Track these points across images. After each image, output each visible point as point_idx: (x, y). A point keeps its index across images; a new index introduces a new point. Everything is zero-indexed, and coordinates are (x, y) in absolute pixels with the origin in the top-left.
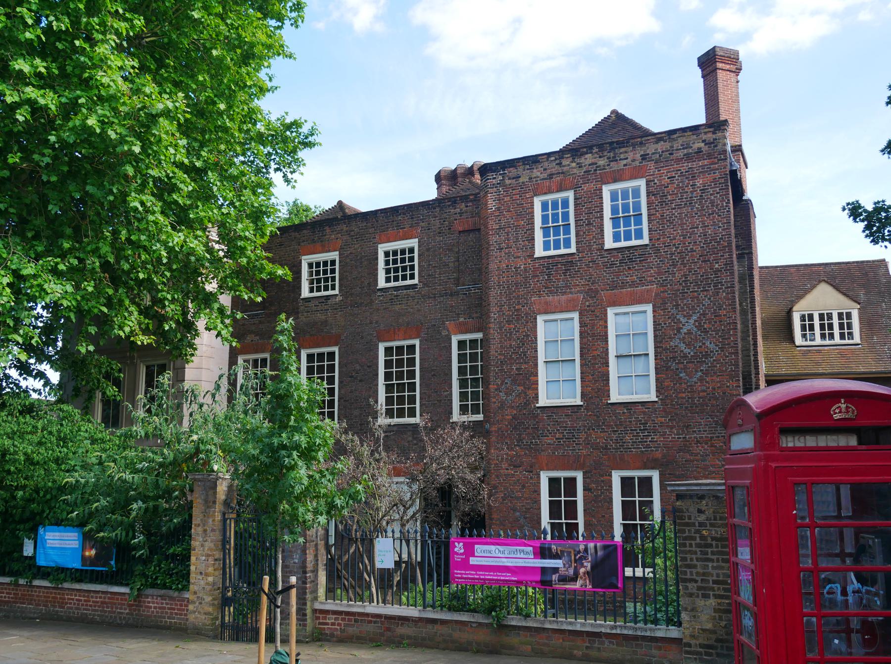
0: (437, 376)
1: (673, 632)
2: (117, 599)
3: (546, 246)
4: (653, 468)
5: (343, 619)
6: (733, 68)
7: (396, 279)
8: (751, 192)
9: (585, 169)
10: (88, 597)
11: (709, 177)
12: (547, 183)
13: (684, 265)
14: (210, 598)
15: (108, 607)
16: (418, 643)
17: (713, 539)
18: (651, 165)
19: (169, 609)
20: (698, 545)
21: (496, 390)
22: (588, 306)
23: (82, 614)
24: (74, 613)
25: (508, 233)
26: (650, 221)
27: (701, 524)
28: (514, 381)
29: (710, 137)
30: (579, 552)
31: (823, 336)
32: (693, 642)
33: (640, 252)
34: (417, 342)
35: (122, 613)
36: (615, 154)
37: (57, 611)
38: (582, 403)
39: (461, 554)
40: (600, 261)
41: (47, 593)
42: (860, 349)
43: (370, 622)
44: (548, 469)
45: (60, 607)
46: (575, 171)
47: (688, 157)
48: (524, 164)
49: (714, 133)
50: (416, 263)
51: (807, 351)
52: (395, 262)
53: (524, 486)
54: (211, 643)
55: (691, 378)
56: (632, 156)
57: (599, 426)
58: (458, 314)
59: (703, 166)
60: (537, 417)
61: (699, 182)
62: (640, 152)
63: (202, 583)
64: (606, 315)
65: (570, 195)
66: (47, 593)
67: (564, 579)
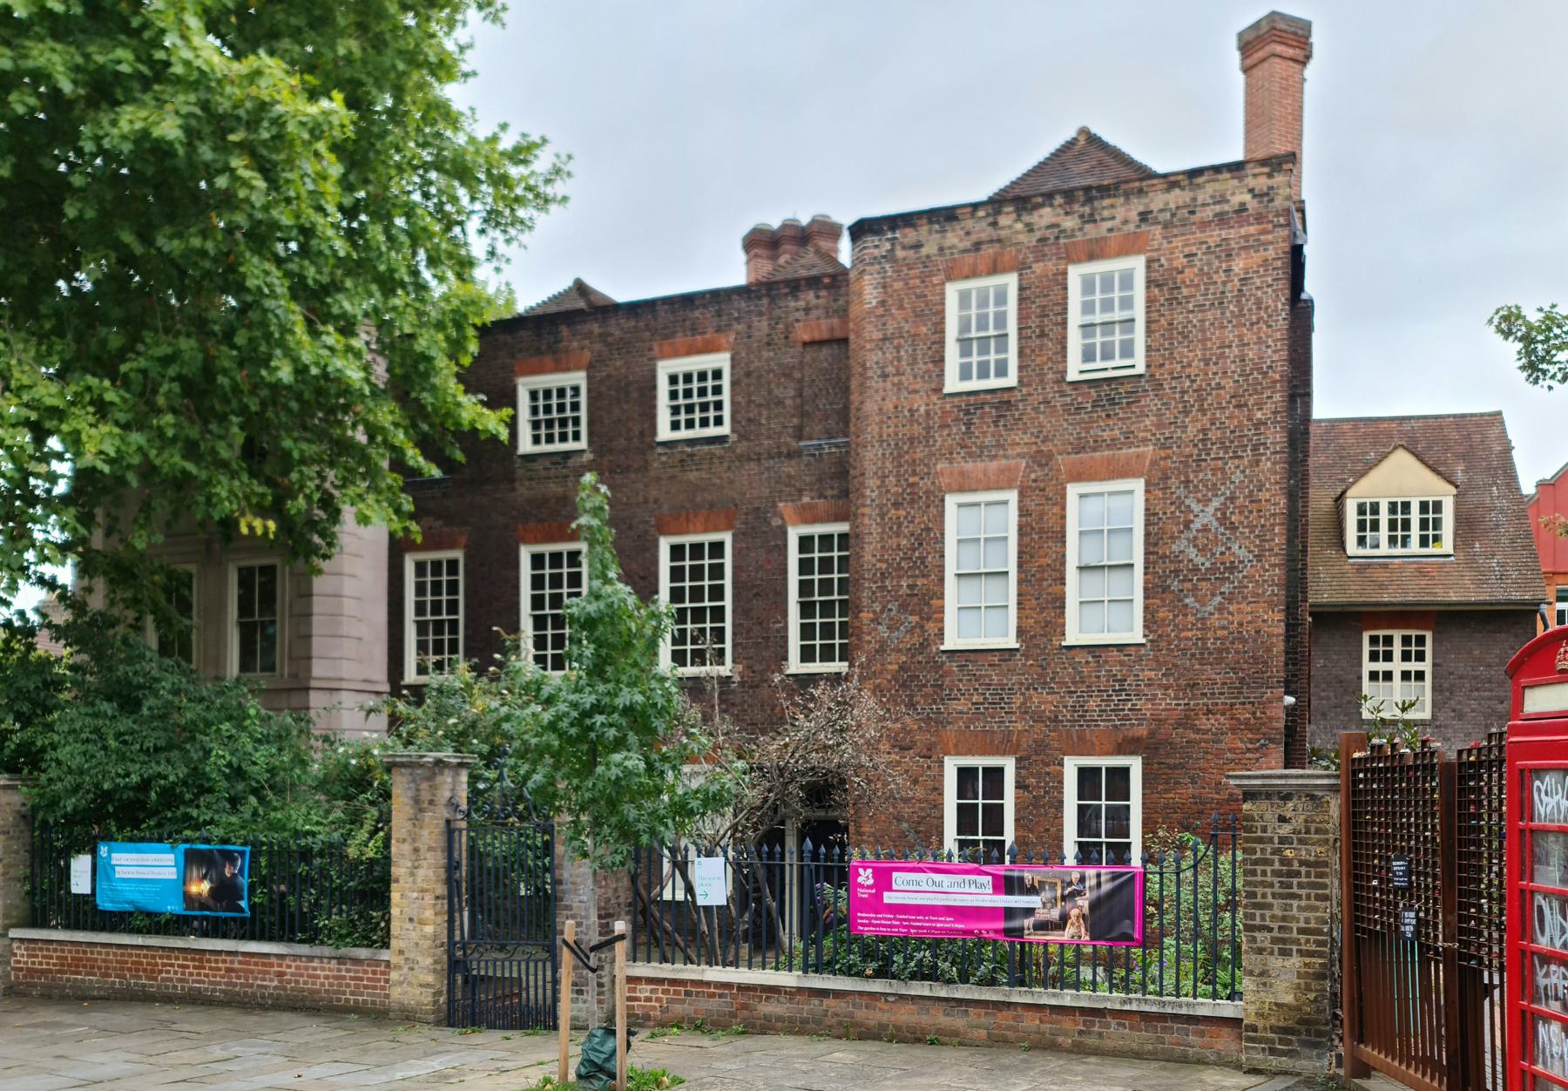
0: (761, 595)
1: (1227, 1009)
2: (131, 955)
3: (965, 374)
4: (1132, 753)
5: (665, 992)
6: (1297, 53)
7: (690, 424)
8: (1311, 288)
9: (1038, 235)
10: (201, 960)
11: (1256, 257)
12: (969, 258)
13: (1202, 411)
14: (429, 961)
15: (238, 978)
16: (798, 1027)
17: (1302, 863)
18: (1157, 231)
19: (352, 978)
20: (1276, 873)
22: (1035, 481)
23: (190, 989)
24: (175, 987)
26: (1149, 332)
27: (1282, 840)
28: (903, 607)
29: (1262, 183)
31: (1392, 541)
32: (1260, 1024)
33: (1128, 387)
34: (727, 538)
35: (266, 987)
36: (1093, 209)
37: (144, 986)
39: (869, 887)
40: (1058, 402)
41: (122, 955)
43: (712, 995)
44: (958, 754)
45: (148, 978)
46: (1023, 238)
48: (931, 222)
49: (1270, 176)
50: (726, 396)
51: (1364, 567)
54: (1115, 1066)
55: (1204, 605)
56: (1121, 213)
59: (1246, 237)
62: (1137, 205)
63: (414, 935)
64: (1064, 497)
65: (1011, 281)
66: (122, 955)
67: (1042, 926)
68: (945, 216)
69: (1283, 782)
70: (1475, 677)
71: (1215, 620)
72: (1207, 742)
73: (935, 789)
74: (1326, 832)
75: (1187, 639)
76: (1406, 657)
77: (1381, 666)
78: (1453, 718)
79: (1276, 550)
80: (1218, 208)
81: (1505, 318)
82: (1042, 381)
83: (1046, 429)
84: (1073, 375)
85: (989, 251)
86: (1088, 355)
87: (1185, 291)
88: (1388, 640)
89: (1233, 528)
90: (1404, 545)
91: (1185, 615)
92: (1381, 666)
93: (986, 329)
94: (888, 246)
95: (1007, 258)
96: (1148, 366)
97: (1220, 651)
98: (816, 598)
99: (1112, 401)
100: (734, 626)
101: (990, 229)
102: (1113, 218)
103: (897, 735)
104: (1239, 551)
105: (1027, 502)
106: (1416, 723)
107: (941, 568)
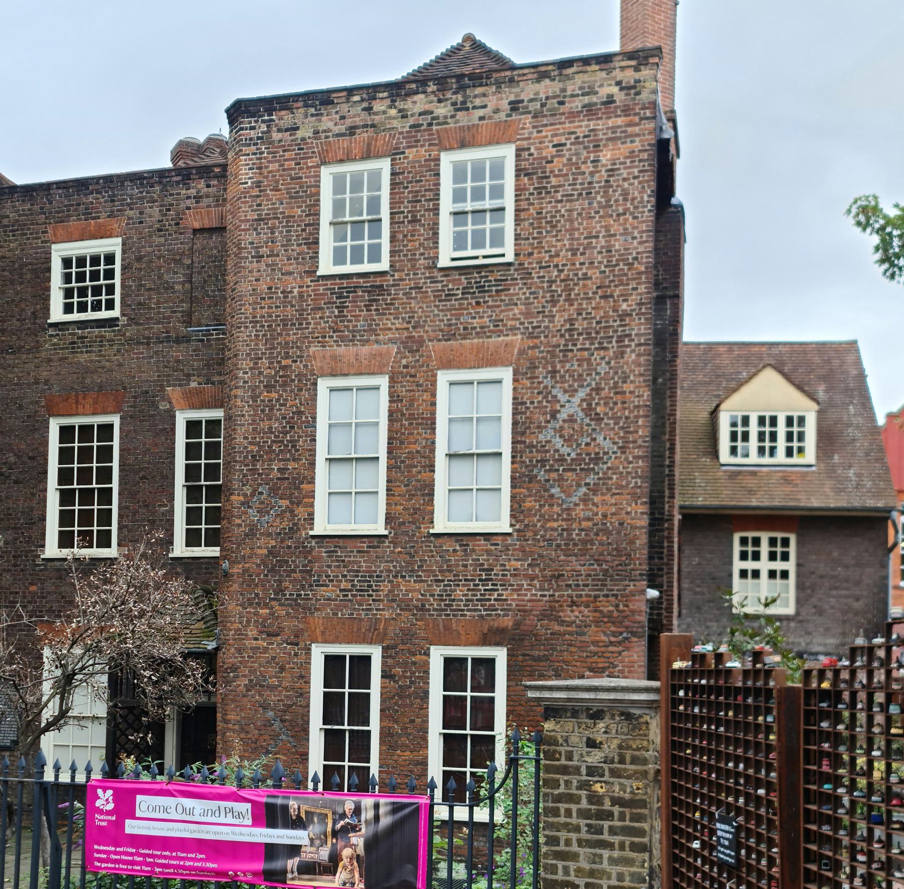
0: (148, 479)
3: (339, 258)
4: (498, 644)
7: (82, 308)
8: (681, 194)
9: (412, 121)
11: (624, 149)
12: (344, 142)
17: (615, 801)
18: (527, 120)
20: (583, 814)
21: (243, 504)
22: (406, 367)
25: (272, 230)
26: (518, 221)
27: (591, 771)
28: (274, 491)
29: (629, 76)
30: (343, 816)
31: (761, 451)
33: (498, 275)
34: (115, 420)
36: (465, 97)
38: (386, 533)
39: (109, 813)
40: (429, 288)
42: (813, 472)
44: (325, 641)
46: (395, 123)
47: (590, 110)
48: (306, 106)
49: (637, 69)
50: (117, 281)
51: (735, 474)
52: (81, 277)
53: (282, 669)
55: (569, 496)
56: (493, 101)
57: (413, 571)
58: (188, 375)
59: (614, 129)
60: (310, 552)
61: (606, 156)
62: (509, 95)
64: (434, 383)
65: (384, 166)
68: (320, 100)
69: (591, 695)
70: (834, 577)
71: (580, 512)
72: (571, 634)
73: (302, 677)
74: (645, 762)
75: (553, 529)
76: (772, 557)
77: (750, 565)
78: (814, 614)
79: (640, 442)
80: (586, 100)
81: (864, 210)
82: (413, 266)
83: (416, 314)
84: (444, 261)
85: (363, 136)
86: (459, 242)
87: (554, 181)
88: (757, 542)
89: (598, 419)
90: (772, 454)
91: (551, 505)
92: (750, 565)
93: (361, 214)
94: (264, 128)
95: (380, 143)
96: (517, 255)
97: (584, 542)
98: (203, 483)
99: (482, 289)
100: (120, 508)
101: (364, 115)
102: (485, 107)
103: (265, 620)
104: (604, 442)
105: (398, 387)
106: (780, 618)
107: (312, 452)
